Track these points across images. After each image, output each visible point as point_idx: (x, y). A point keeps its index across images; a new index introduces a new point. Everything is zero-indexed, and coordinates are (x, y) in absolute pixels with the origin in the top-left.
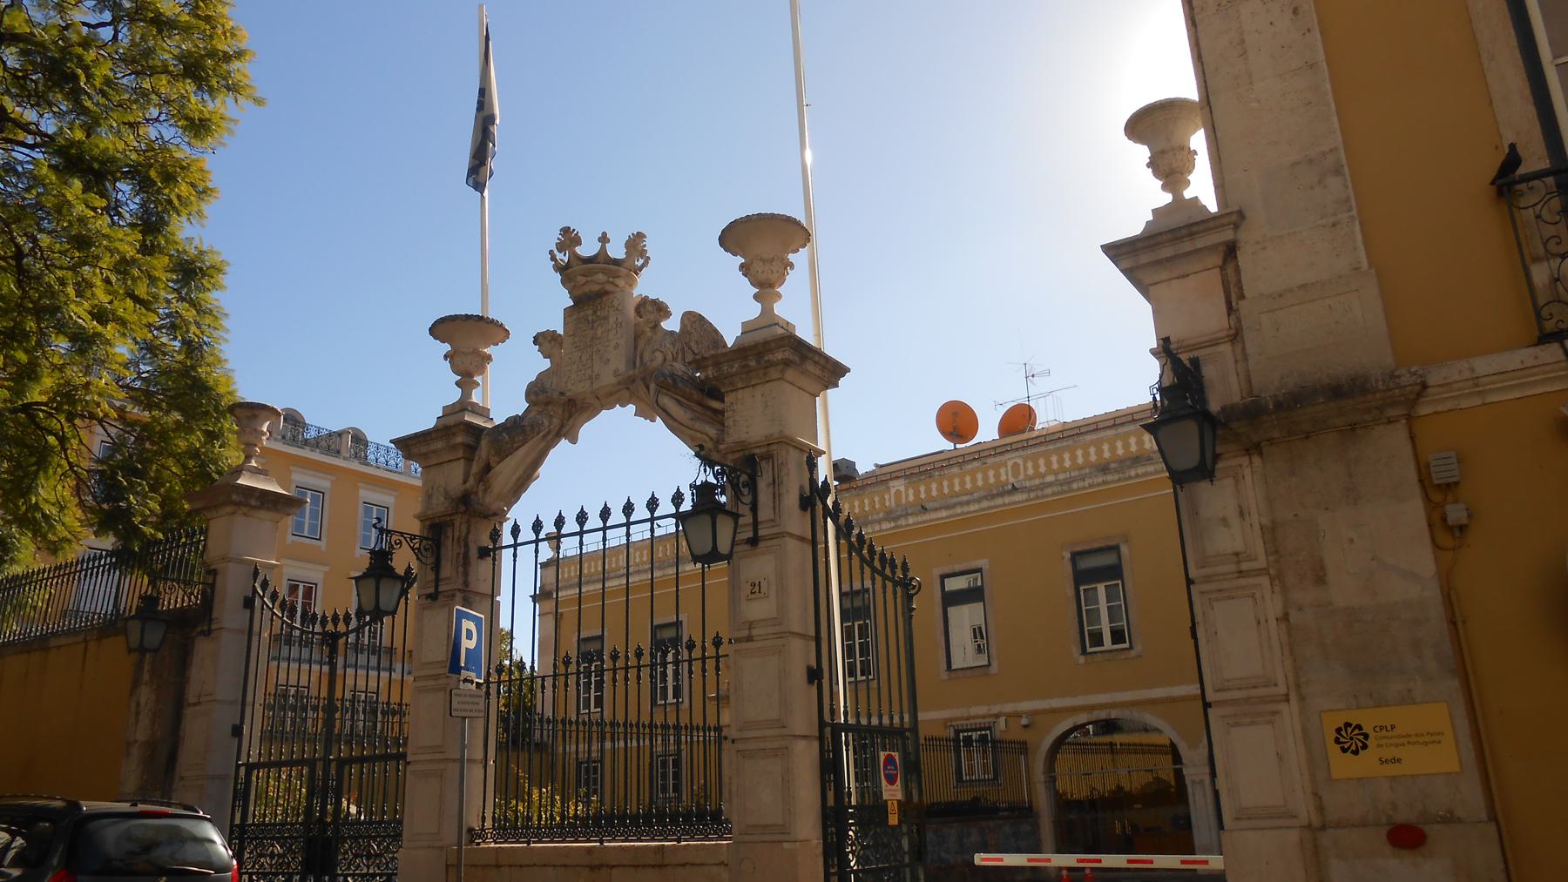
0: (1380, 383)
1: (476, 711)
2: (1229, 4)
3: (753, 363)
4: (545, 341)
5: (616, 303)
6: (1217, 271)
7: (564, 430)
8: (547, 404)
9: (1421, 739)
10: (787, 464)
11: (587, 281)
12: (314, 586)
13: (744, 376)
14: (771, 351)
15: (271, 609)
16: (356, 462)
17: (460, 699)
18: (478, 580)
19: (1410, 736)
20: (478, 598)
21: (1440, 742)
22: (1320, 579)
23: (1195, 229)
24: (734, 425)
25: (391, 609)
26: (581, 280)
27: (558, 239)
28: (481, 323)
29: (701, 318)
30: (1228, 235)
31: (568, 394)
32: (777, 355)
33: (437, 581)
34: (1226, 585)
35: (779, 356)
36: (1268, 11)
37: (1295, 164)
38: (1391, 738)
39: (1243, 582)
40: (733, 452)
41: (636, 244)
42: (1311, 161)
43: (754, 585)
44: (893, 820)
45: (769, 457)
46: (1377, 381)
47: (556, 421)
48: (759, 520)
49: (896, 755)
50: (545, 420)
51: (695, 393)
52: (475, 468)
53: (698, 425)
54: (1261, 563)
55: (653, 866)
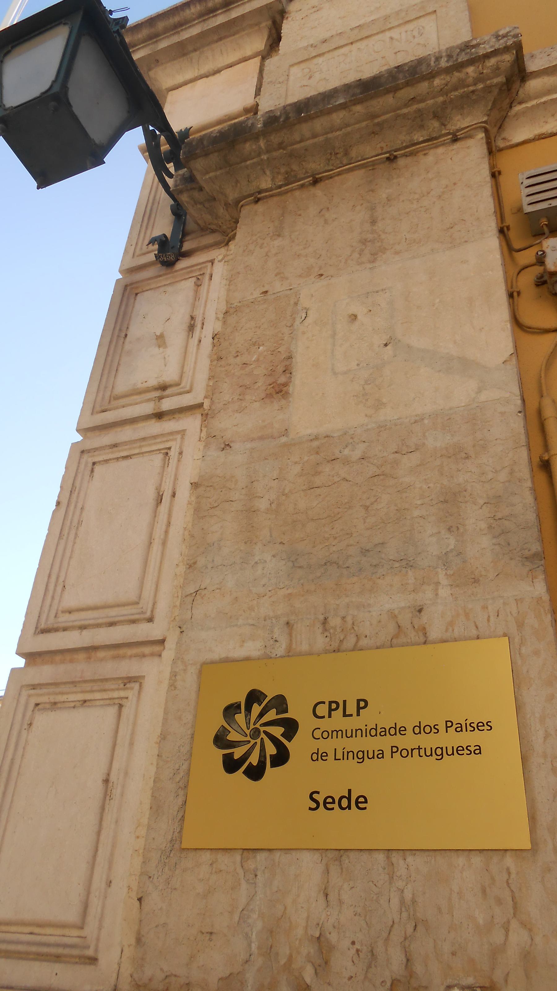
19: (402, 731)
21: (479, 750)
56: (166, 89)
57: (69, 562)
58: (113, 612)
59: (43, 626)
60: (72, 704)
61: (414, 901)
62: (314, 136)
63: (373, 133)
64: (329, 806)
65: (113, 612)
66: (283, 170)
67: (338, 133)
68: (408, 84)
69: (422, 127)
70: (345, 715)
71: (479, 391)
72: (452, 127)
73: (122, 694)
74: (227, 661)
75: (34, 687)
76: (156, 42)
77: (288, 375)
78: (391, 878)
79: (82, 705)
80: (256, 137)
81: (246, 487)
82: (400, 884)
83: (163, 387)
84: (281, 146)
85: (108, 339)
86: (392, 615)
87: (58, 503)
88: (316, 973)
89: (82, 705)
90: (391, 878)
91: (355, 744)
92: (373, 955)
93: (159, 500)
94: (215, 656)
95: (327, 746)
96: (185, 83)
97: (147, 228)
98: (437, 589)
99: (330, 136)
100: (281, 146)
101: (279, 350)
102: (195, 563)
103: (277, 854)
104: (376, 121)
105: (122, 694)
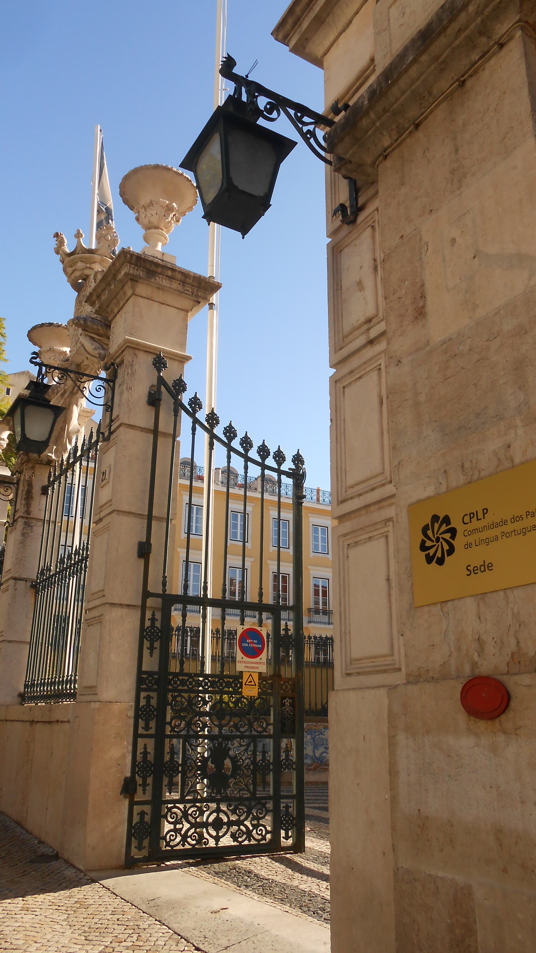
9: (518, 526)
10: (132, 365)
12: (288, 576)
14: (118, 271)
28: (52, 327)
51: (100, 328)
56: (321, 57)
57: (345, 456)
58: (372, 482)
59: (340, 499)
60: (364, 541)
61: (518, 613)
62: (404, 93)
63: (442, 70)
64: (475, 572)
65: (372, 482)
66: (394, 127)
67: (418, 82)
68: (450, 21)
69: (475, 47)
70: (478, 520)
71: (530, 279)
72: (496, 37)
73: (386, 529)
74: (419, 501)
75: (345, 535)
76: (300, 24)
77: (424, 299)
78: (507, 603)
79: (369, 540)
80: (367, 113)
81: (413, 388)
82: (512, 605)
83: (369, 321)
84: (385, 111)
85: (332, 295)
86: (495, 453)
87: (331, 420)
88: (479, 655)
89: (369, 540)
90: (507, 603)
91: (484, 535)
92: (502, 642)
94: (413, 500)
95: (471, 539)
96: (332, 45)
97: (335, 193)
98: (516, 431)
99: (413, 87)
100: (385, 111)
101: (416, 281)
102: (396, 445)
103: (456, 601)
104: (440, 61)
105: (386, 529)
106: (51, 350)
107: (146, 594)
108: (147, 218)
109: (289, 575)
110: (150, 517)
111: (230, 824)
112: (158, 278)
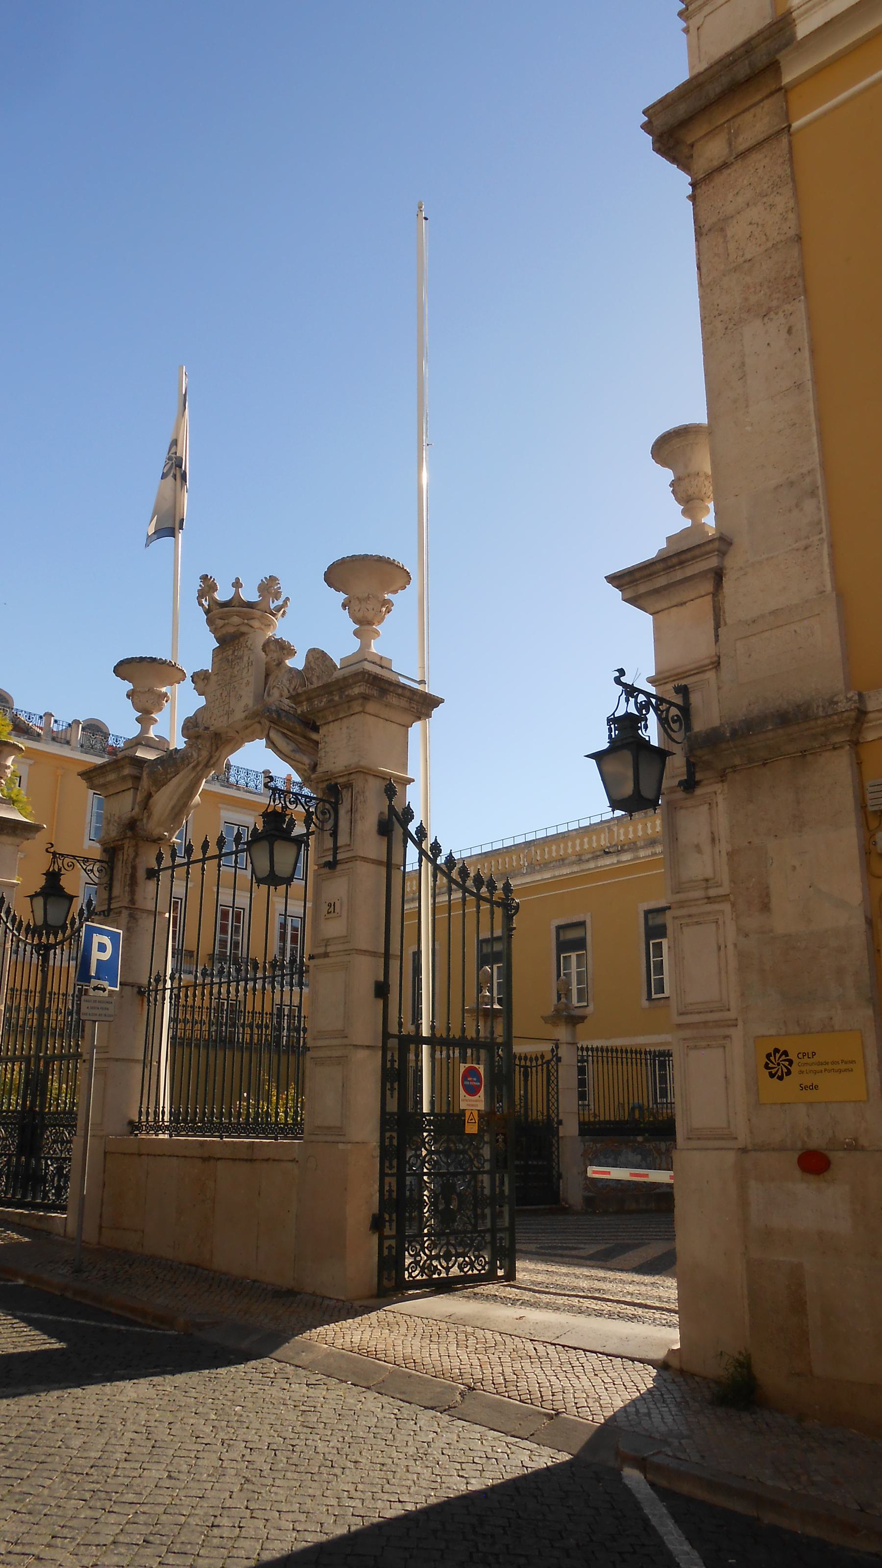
0: (821, 709)
1: (105, 1015)
2: (735, 327)
3: (337, 698)
4: (200, 679)
5: (249, 644)
6: (709, 598)
7: (212, 762)
8: (198, 737)
9: (836, 1067)
11: (224, 625)
12: (242, 911)
13: (332, 710)
14: (350, 686)
15: (5, 923)
16: (218, 784)
17: (89, 1005)
18: (145, 898)
19: (827, 1063)
20: (145, 915)
21: (852, 1070)
22: (766, 907)
23: (683, 557)
24: (325, 756)
25: (60, 923)
26: (220, 623)
27: (200, 586)
28: (155, 663)
29: (323, 654)
30: (713, 562)
31: (212, 728)
32: (354, 689)
33: (110, 899)
34: (694, 910)
35: (356, 691)
36: (767, 332)
37: (780, 486)
38: (812, 1064)
39: (709, 908)
40: (323, 781)
41: (269, 587)
42: (792, 484)
43: (330, 905)
44: (471, 1128)
45: (349, 786)
46: (818, 707)
47: (205, 753)
48: (338, 845)
49: (481, 1069)
50: (194, 753)
51: (297, 726)
52: (139, 797)
53: (298, 756)
54: (724, 890)
55: (246, 1160)
93: (719, 949)
95: (804, 1069)
106: (151, 691)
107: (386, 1035)
108: (361, 612)
109: (244, 909)
110: (387, 955)
111: (458, 1256)
112: (388, 696)
